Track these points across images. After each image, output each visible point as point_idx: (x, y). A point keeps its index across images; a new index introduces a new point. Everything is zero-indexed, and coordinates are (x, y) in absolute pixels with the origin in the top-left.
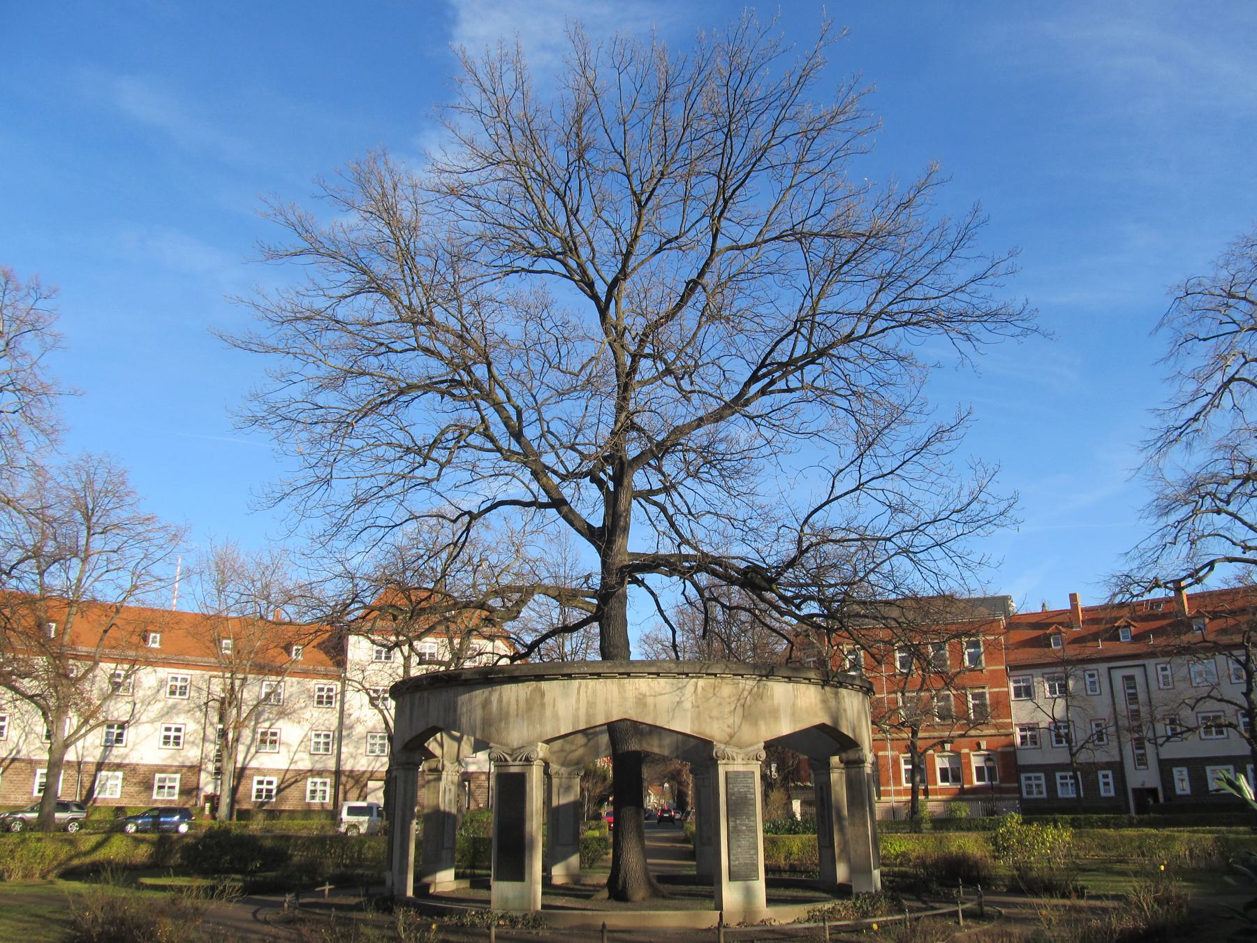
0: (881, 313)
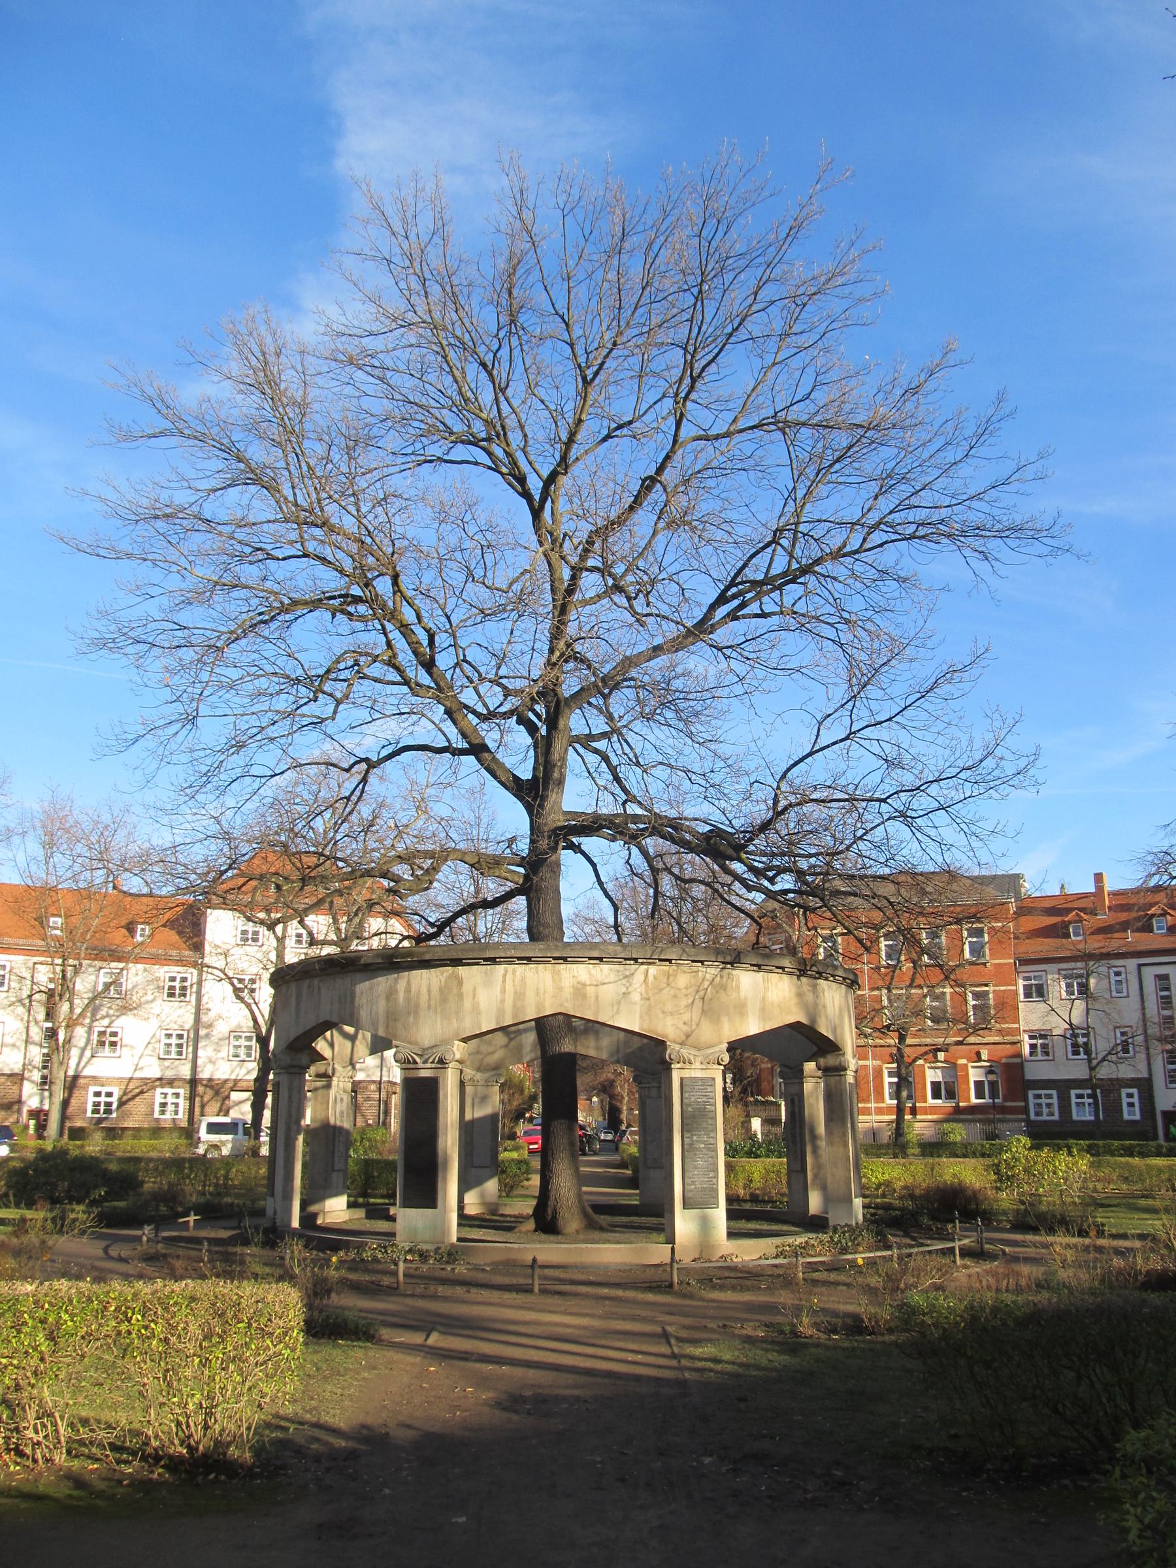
0: (879, 523)
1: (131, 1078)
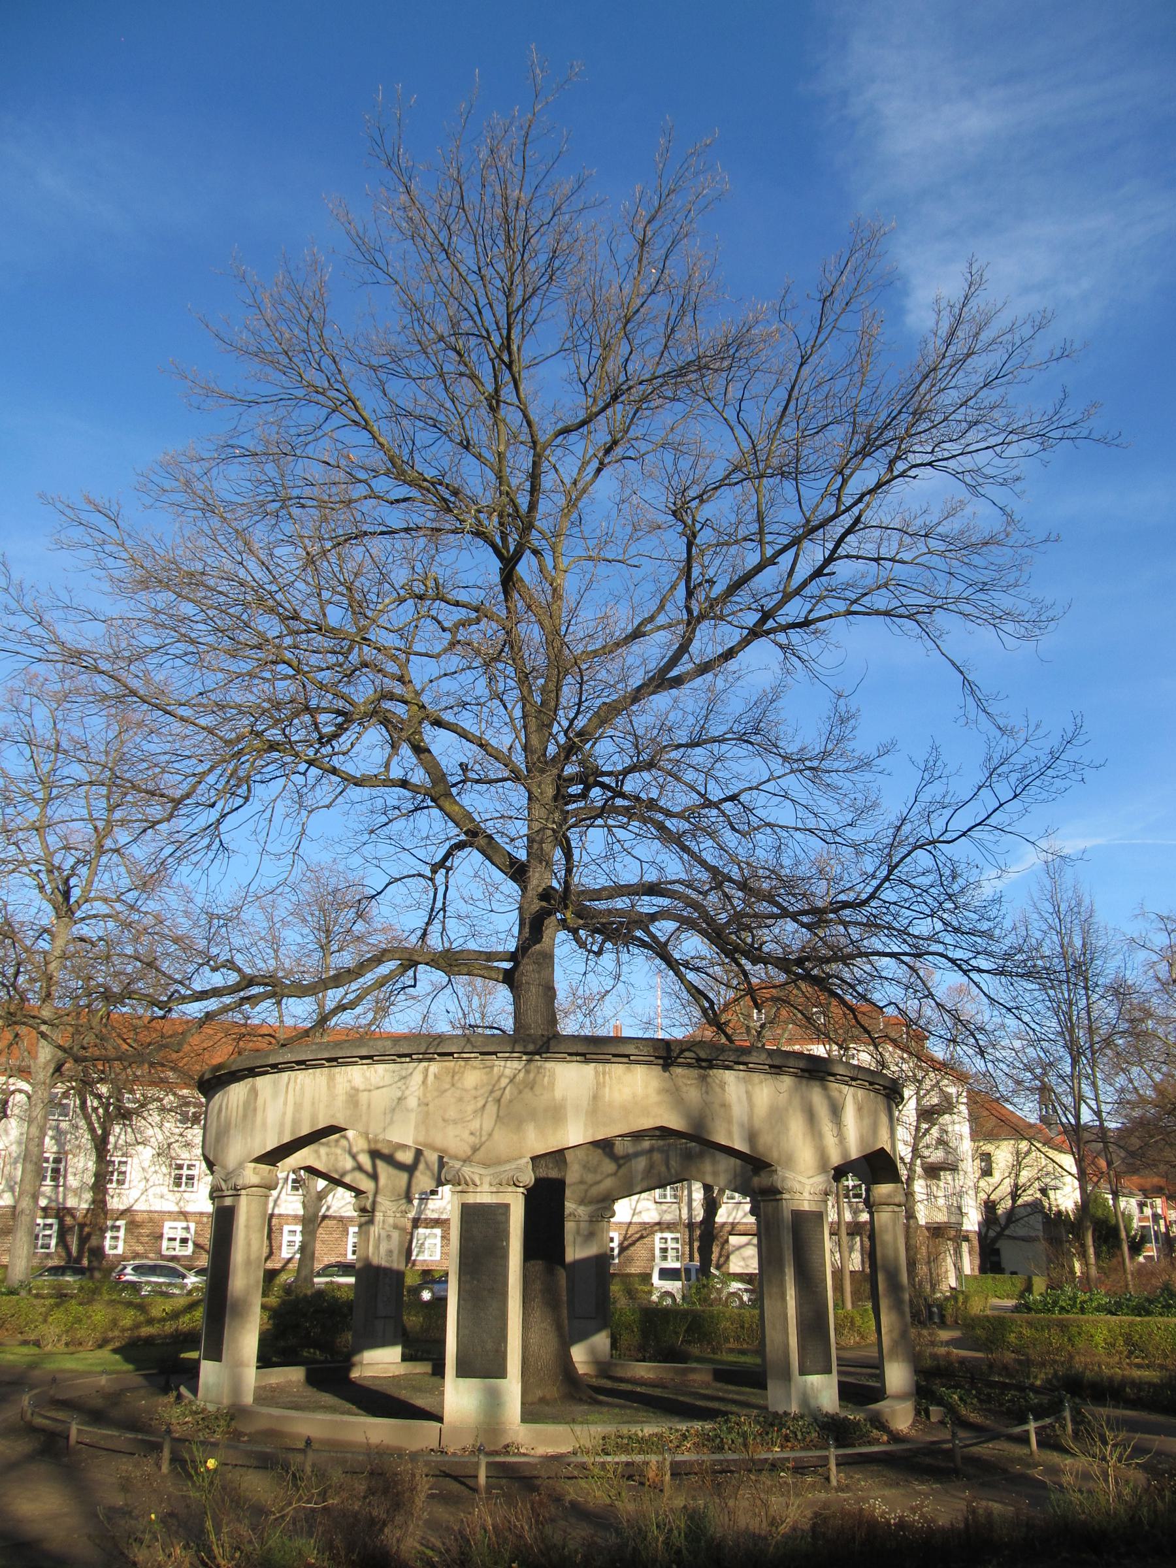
1: (630, 1223)
